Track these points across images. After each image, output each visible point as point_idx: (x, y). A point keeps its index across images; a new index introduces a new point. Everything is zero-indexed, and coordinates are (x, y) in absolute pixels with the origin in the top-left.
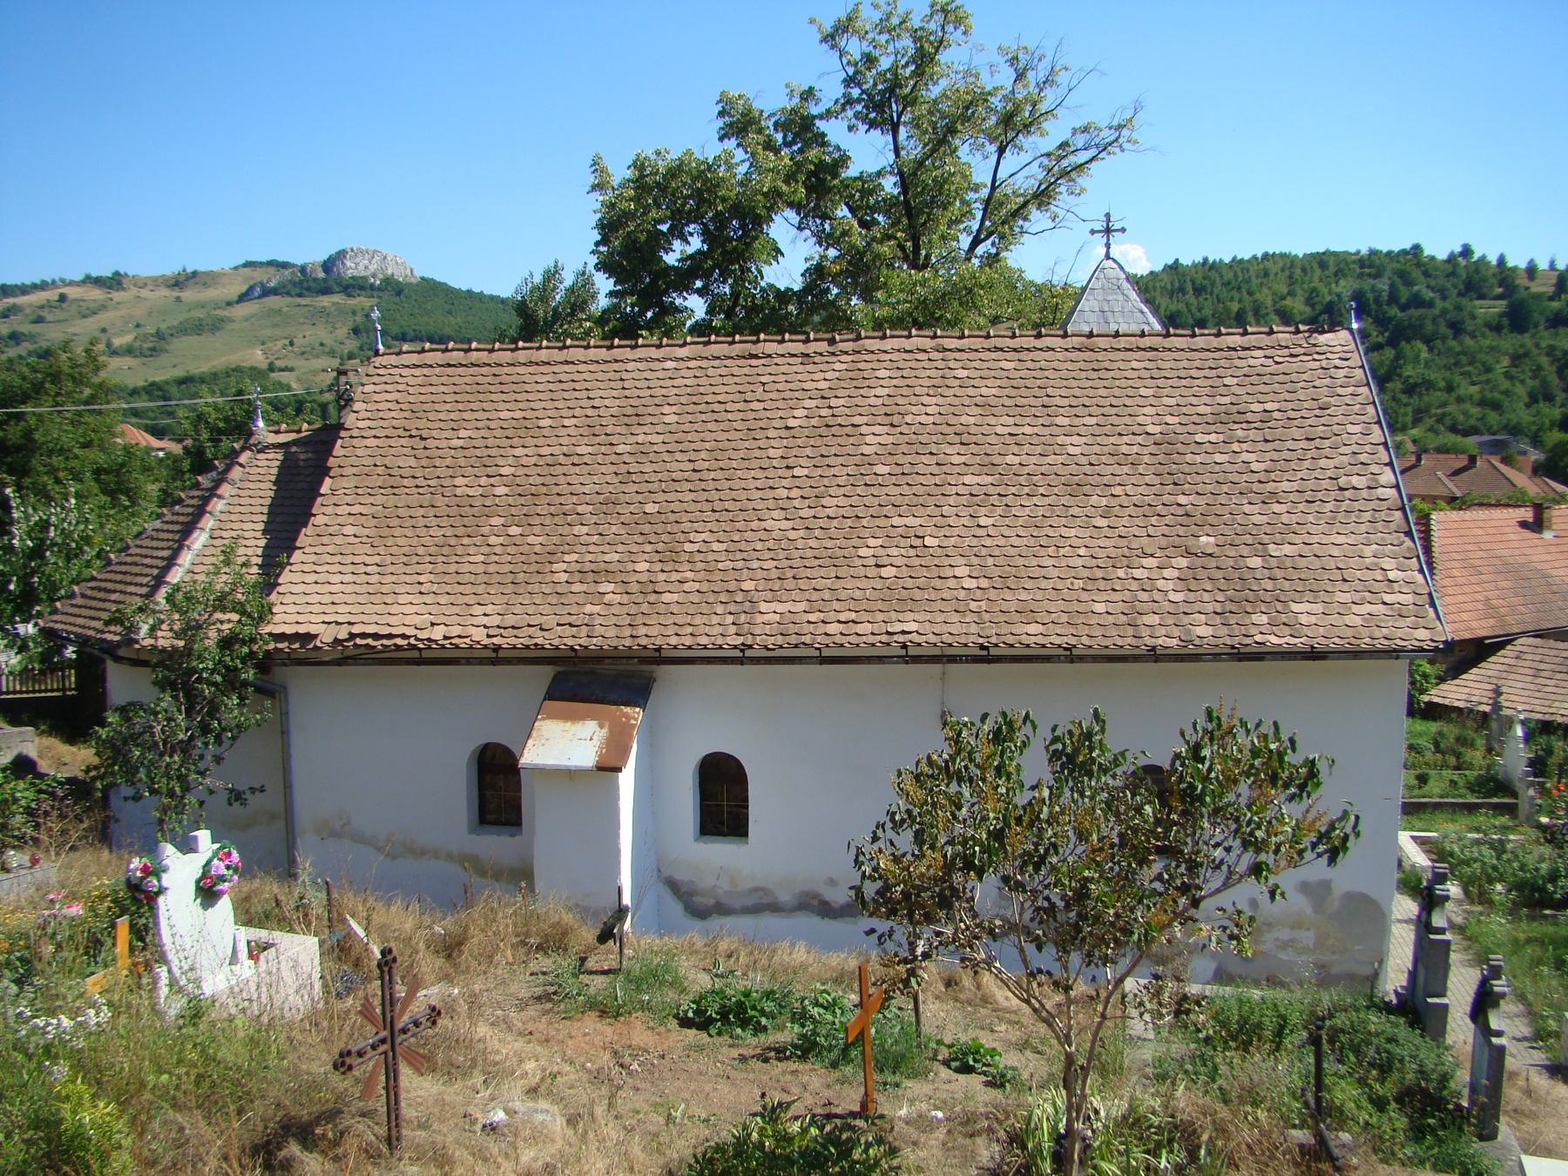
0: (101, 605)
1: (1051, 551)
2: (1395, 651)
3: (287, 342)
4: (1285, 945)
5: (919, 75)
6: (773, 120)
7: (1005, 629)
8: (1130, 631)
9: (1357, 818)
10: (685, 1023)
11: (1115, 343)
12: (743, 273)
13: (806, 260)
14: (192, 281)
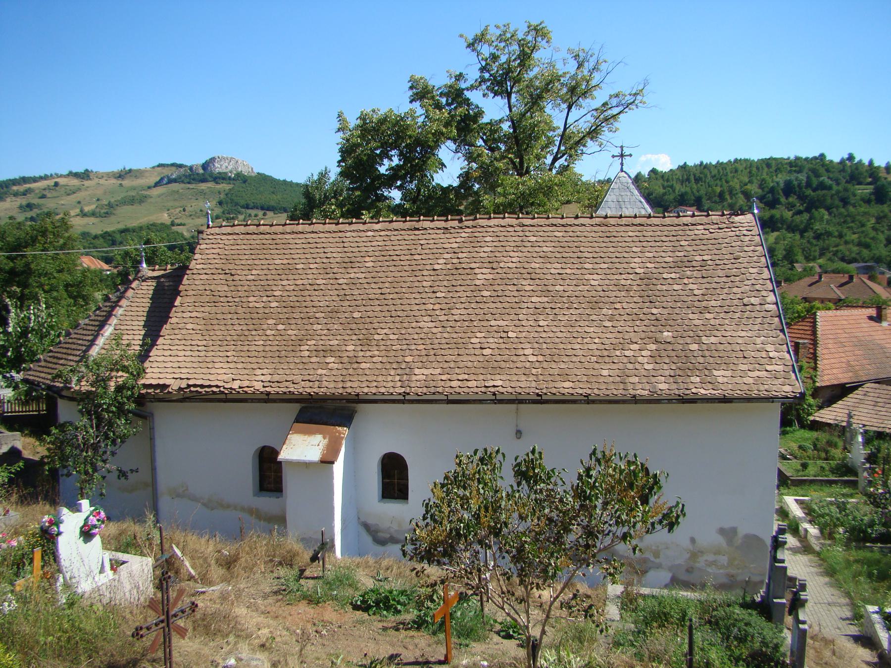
0: (54, 366)
1: (579, 340)
3: (182, 209)
5: (522, 66)
6: (440, 91)
7: (551, 385)
8: (622, 386)
9: (683, 505)
10: (356, 607)
11: (620, 221)
12: (422, 177)
13: (461, 169)
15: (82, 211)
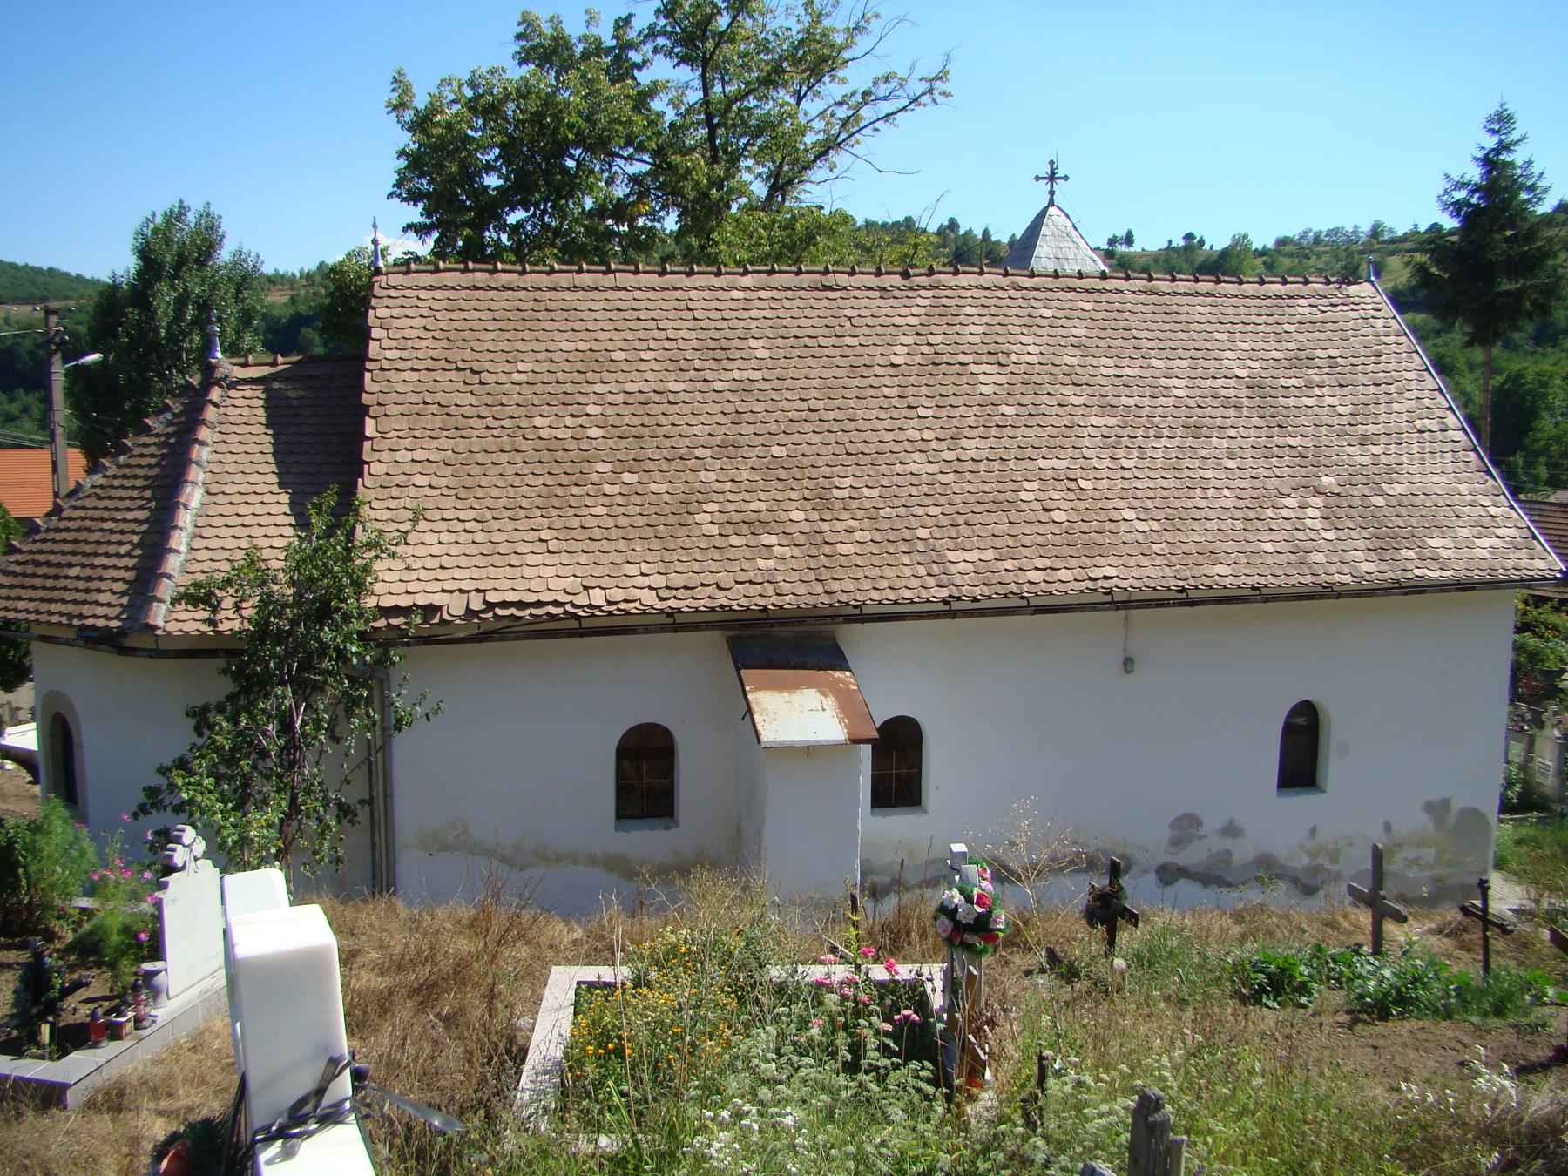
4: (1414, 862)
7: (1198, 571)
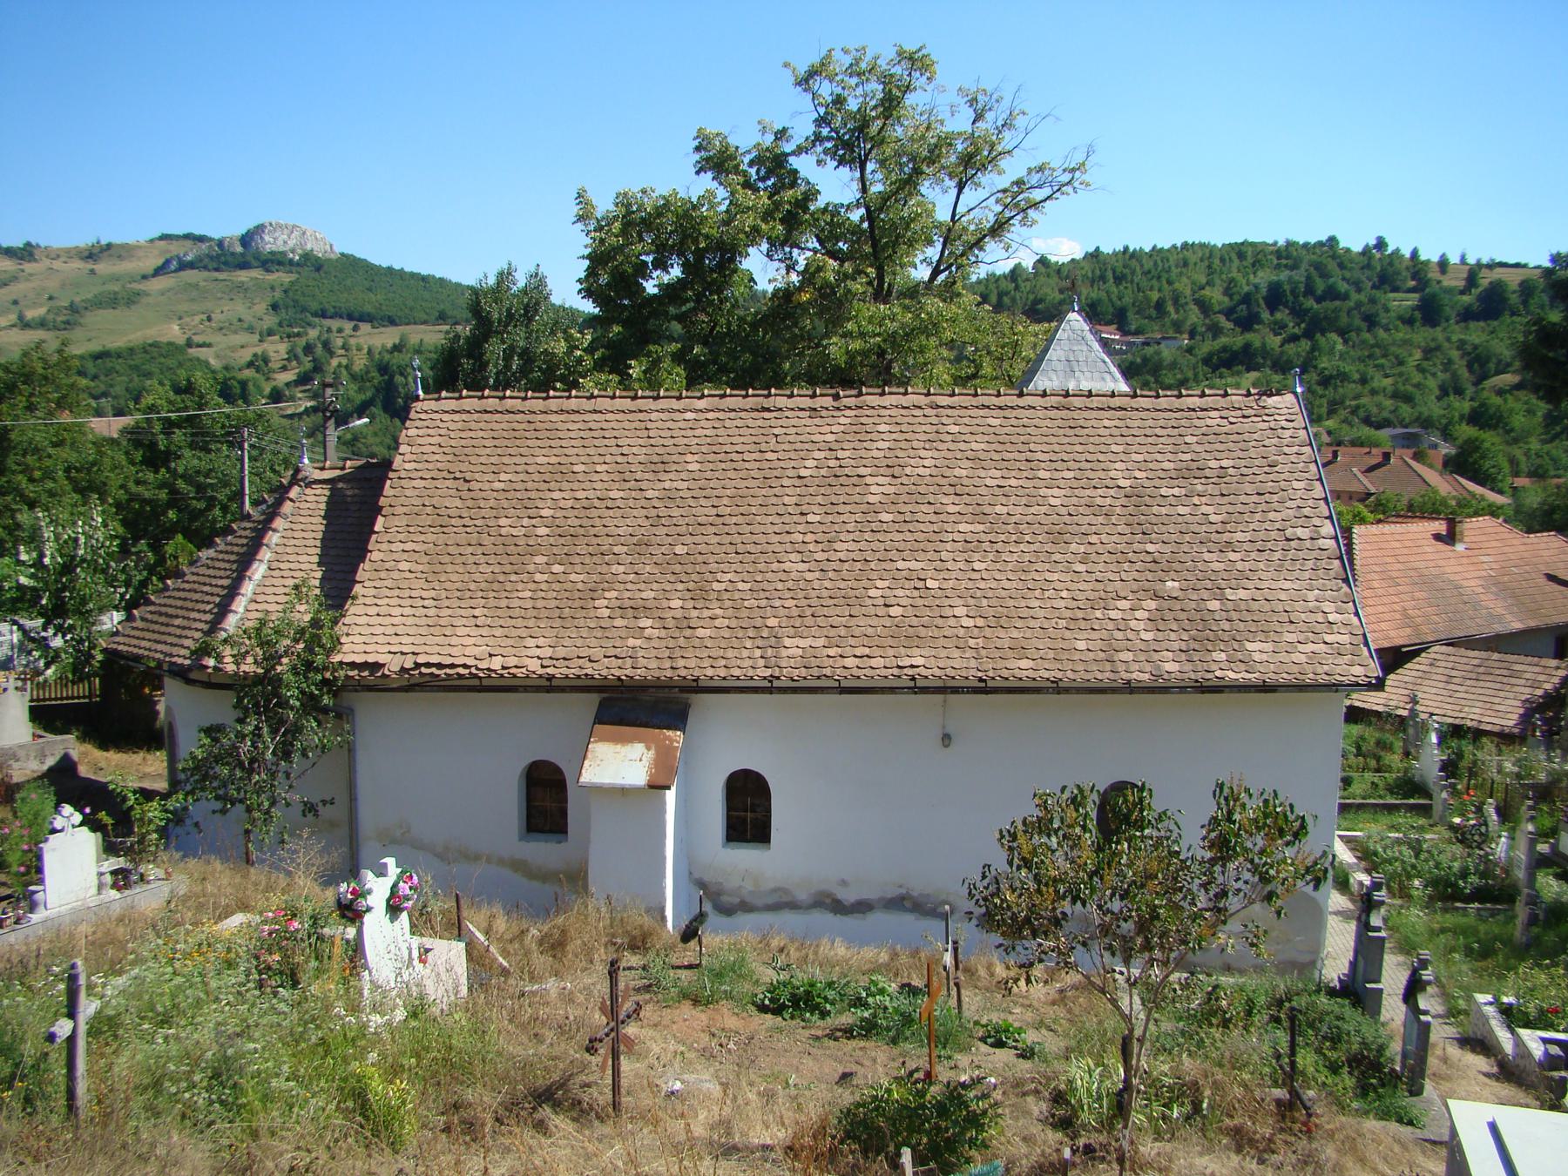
1: (1037, 594)
2: (1334, 685)
3: (204, 317)
8: (1108, 666)
10: (763, 1009)
14: (106, 254)
15: (21, 317)
